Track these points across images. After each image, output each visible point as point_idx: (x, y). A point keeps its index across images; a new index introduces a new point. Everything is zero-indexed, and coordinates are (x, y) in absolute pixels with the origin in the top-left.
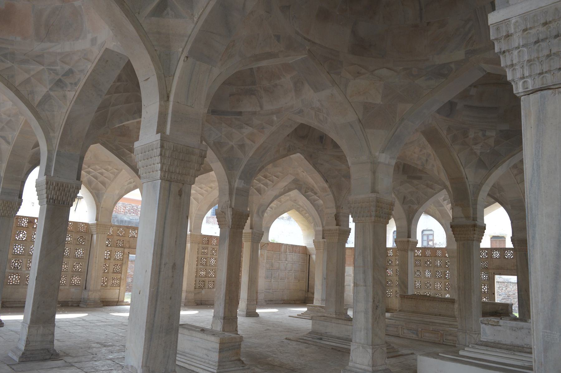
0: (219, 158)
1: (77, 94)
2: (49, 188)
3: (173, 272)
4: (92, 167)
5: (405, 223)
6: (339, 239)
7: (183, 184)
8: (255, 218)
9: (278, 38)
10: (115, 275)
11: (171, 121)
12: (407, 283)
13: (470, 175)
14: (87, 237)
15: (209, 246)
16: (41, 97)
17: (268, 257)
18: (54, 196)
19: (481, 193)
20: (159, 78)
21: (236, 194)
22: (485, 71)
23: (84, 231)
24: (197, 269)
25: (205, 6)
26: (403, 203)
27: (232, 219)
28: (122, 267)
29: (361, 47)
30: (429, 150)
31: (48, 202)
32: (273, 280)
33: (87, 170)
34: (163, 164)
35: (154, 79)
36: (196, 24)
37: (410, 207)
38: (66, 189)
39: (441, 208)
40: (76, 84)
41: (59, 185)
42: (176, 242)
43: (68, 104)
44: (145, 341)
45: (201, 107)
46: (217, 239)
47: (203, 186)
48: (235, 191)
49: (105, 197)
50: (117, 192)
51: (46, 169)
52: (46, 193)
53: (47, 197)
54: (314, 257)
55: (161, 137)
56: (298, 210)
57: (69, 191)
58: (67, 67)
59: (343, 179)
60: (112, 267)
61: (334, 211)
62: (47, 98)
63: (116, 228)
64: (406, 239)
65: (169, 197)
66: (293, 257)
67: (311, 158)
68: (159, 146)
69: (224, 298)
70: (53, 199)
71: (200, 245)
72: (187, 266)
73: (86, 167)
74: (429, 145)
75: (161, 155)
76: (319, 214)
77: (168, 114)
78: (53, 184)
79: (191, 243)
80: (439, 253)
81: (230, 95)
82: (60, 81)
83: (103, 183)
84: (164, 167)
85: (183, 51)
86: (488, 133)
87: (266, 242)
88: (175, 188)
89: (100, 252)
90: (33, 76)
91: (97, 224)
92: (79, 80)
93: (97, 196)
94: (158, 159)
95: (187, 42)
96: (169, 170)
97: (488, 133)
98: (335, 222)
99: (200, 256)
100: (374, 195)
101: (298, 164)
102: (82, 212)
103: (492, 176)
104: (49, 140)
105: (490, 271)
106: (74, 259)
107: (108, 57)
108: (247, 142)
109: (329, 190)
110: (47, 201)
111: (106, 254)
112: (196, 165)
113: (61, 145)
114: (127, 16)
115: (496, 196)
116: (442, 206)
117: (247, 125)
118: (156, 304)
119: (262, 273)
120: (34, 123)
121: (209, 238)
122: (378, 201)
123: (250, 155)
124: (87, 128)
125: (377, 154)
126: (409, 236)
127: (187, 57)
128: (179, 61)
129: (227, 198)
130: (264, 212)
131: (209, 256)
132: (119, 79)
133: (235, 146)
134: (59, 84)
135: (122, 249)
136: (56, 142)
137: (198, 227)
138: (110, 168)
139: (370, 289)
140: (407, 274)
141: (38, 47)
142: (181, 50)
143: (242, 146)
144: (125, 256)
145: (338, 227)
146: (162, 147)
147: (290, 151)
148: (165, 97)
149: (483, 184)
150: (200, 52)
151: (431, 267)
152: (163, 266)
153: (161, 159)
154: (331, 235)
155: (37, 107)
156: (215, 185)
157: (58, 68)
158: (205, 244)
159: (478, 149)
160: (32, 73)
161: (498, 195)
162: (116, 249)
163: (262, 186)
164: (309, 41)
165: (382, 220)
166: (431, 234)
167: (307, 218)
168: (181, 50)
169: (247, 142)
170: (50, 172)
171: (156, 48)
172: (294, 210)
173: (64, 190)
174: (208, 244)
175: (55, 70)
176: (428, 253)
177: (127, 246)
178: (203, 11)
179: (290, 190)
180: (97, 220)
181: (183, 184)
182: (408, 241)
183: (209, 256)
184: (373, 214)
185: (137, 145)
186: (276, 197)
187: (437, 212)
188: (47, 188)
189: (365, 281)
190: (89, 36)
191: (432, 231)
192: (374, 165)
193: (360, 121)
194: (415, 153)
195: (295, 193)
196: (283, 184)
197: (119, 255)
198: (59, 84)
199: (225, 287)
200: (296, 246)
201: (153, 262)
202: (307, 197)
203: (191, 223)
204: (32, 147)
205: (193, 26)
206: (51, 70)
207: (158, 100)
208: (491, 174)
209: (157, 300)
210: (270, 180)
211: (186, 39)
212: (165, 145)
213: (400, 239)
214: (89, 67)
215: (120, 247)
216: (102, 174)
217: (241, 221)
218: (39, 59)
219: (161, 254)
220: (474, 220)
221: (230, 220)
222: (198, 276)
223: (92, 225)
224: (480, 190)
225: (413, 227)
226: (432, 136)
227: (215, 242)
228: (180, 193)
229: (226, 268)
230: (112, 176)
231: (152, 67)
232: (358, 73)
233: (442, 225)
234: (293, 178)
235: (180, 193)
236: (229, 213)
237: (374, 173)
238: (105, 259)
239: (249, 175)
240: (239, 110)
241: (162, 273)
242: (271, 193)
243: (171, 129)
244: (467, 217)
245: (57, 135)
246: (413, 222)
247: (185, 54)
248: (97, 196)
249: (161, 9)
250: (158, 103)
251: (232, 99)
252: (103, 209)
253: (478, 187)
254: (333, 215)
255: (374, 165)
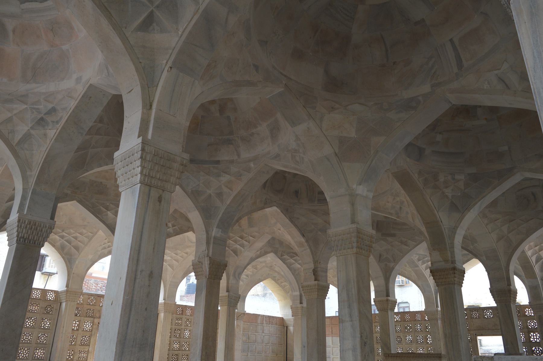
0: (196, 207)
1: (58, 131)
2: (21, 226)
3: (149, 280)
4: (66, 232)
5: (382, 281)
6: (318, 295)
7: (163, 191)
8: (232, 281)
9: (256, 68)
10: (82, 347)
11: (153, 126)
12: (390, 344)
13: (445, 219)
14: (55, 305)
15: (184, 316)
16: (21, 136)
17: (244, 329)
18: (26, 235)
19: (456, 236)
20: (143, 88)
21: (214, 243)
22: (451, 103)
23: (52, 304)
24: (170, 341)
25: (189, 20)
26: (379, 261)
27: (210, 268)
28: (90, 339)
29: (334, 85)
30: (403, 196)
31: (18, 241)
32: (249, 354)
33: (61, 234)
34: (143, 167)
35: (138, 90)
36: (181, 37)
37: (386, 265)
38: (38, 228)
39: (417, 268)
40: (57, 122)
41: (32, 224)
42: (154, 249)
43: (48, 143)
44: (115, 355)
45: (183, 120)
46: (191, 309)
47: (179, 252)
48: (212, 240)
49: (77, 262)
50: (90, 257)
51: (19, 207)
52: (17, 231)
53: (18, 236)
54: (291, 328)
55: (142, 140)
56: (274, 279)
57: (42, 231)
58: (50, 106)
59: (320, 233)
60: (80, 338)
61: (312, 266)
62: (27, 137)
63: (87, 296)
64: (385, 298)
65: (148, 202)
66: (270, 329)
67: (287, 211)
68: (140, 149)
69: (200, 354)
70: (23, 237)
71: (174, 315)
72: (160, 337)
73: (61, 231)
74: (403, 192)
75: (141, 158)
76: (296, 279)
77: (150, 121)
78: (25, 223)
79: (165, 312)
80: (418, 317)
81: (208, 145)
82: (42, 119)
83: (77, 248)
84: (145, 171)
85: (167, 62)
86: (457, 177)
87: (243, 312)
88: (155, 194)
89: (69, 322)
90: (15, 114)
91: (67, 291)
92: (61, 118)
93: (69, 258)
94: (138, 163)
95: (171, 54)
96: (149, 174)
97: (457, 177)
98: (313, 277)
99: (174, 327)
100: (354, 226)
101: (274, 222)
102: (50, 278)
103: (465, 218)
104: (25, 178)
105: (472, 332)
106: (40, 330)
107: (92, 94)
108: (225, 190)
109: (306, 244)
110: (17, 240)
111: (75, 324)
112: (177, 173)
113: (37, 183)
114: (114, 29)
115: (469, 249)
116: (417, 266)
117: (225, 173)
118: (130, 314)
119: (238, 345)
120: (12, 163)
121: (184, 308)
122: (359, 232)
123: (228, 203)
124: (65, 167)
125: (354, 186)
126: (388, 295)
127: (171, 68)
128: (162, 72)
129: (204, 247)
130: (240, 274)
131: (183, 327)
132: (100, 120)
133: (212, 194)
134: (41, 122)
135: (92, 319)
136: (32, 181)
137: (171, 294)
138: (84, 231)
139: (357, 324)
140: (389, 335)
141: (23, 88)
142: (165, 62)
143: (220, 195)
144: (94, 327)
145: (316, 282)
146: (143, 150)
147: (267, 204)
148: (148, 105)
149: (457, 227)
150: (183, 64)
151: (411, 332)
152: (139, 273)
153: (142, 162)
154: (309, 300)
155: (16, 145)
156: (192, 250)
157: (41, 107)
158: (179, 314)
159: (449, 192)
160: (15, 112)
161: (472, 247)
162: (86, 318)
163: (238, 247)
164: (285, 76)
165: (363, 252)
166: (407, 307)
167: (283, 287)
168: (164, 62)
169: (225, 190)
170: (23, 210)
171: (141, 61)
172: (270, 279)
173: (36, 229)
174: (182, 314)
175: (38, 109)
176: (407, 317)
177: (97, 315)
178: (188, 24)
179: (266, 253)
180: (67, 286)
181: (163, 191)
182: (387, 300)
183: (183, 327)
184: (355, 245)
185: (116, 154)
186: (252, 260)
187: (413, 274)
188: (18, 226)
189: (351, 316)
190: (75, 76)
191: (410, 297)
192: (353, 198)
193: (336, 155)
194: (388, 202)
195: (270, 258)
196: (259, 244)
197: (88, 326)
198: (41, 122)
199: (201, 341)
200: (273, 317)
201: (128, 267)
202: (284, 261)
203: (165, 287)
204: (6, 199)
205: (177, 39)
206: (34, 108)
207: (141, 108)
208: (464, 216)
209: (131, 310)
210: (246, 241)
211: (170, 51)
212: (146, 148)
213: (379, 299)
214: (73, 104)
215: (89, 317)
216: (76, 238)
217: (218, 279)
218: (23, 98)
219: (138, 260)
220: (452, 263)
221: (208, 270)
222: (171, 349)
223: (62, 292)
224: (455, 233)
225: (390, 285)
226: (404, 179)
227: (188, 312)
228: (160, 199)
229: (203, 321)
230: (86, 240)
231: (136, 77)
232: (332, 108)
233: (419, 287)
234: (269, 237)
235: (160, 199)
236: (206, 262)
237: (353, 204)
238: (73, 330)
239: (227, 224)
240: (217, 159)
241: (137, 281)
242: (248, 254)
243: (152, 134)
244: (446, 261)
245: (34, 173)
246: (391, 280)
247: (170, 64)
248: (69, 261)
249: (148, 24)
250: (141, 111)
251: (211, 131)
252: (75, 275)
253: (453, 231)
254: (311, 271)
255: (353, 198)
